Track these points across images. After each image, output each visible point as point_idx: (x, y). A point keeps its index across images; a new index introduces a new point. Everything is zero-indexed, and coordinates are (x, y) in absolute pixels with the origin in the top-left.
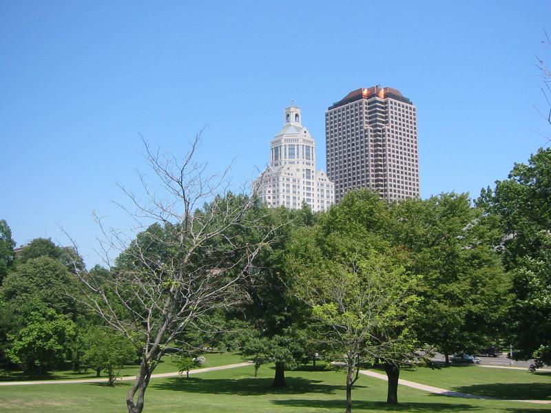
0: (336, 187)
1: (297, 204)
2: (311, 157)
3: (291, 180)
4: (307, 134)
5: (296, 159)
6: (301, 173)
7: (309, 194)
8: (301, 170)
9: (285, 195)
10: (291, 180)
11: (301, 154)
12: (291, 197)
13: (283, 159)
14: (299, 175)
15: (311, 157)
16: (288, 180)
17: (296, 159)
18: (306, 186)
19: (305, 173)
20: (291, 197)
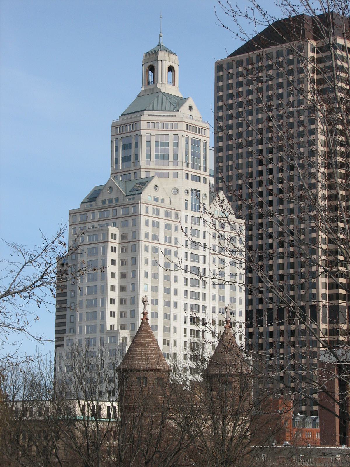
0: (249, 228)
1: (172, 343)
2: (202, 164)
3: (162, 212)
4: (195, 112)
5: (171, 166)
6: (182, 198)
7: (195, 295)
8: (182, 192)
9: (151, 220)
10: (162, 212)
11: (182, 157)
12: (162, 223)
13: (143, 165)
14: (180, 201)
15: (202, 164)
16: (156, 212)
17: (171, 166)
18: (189, 289)
19: (189, 198)
20: (162, 223)
